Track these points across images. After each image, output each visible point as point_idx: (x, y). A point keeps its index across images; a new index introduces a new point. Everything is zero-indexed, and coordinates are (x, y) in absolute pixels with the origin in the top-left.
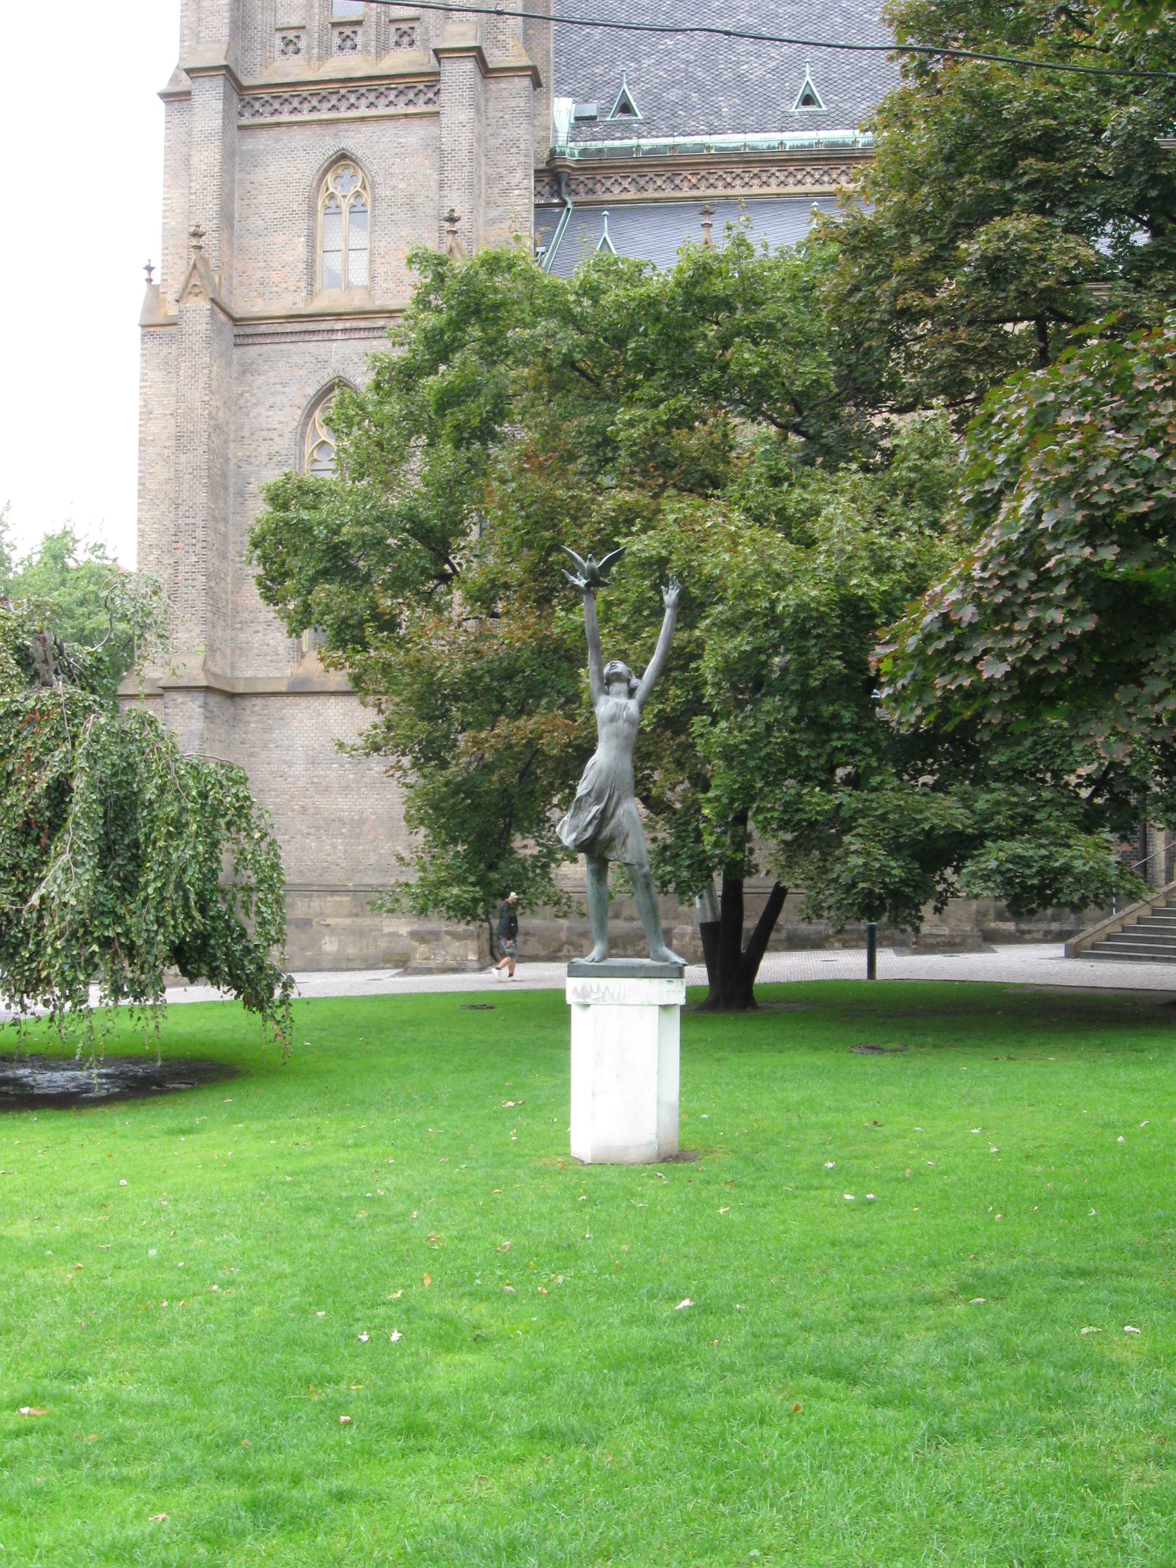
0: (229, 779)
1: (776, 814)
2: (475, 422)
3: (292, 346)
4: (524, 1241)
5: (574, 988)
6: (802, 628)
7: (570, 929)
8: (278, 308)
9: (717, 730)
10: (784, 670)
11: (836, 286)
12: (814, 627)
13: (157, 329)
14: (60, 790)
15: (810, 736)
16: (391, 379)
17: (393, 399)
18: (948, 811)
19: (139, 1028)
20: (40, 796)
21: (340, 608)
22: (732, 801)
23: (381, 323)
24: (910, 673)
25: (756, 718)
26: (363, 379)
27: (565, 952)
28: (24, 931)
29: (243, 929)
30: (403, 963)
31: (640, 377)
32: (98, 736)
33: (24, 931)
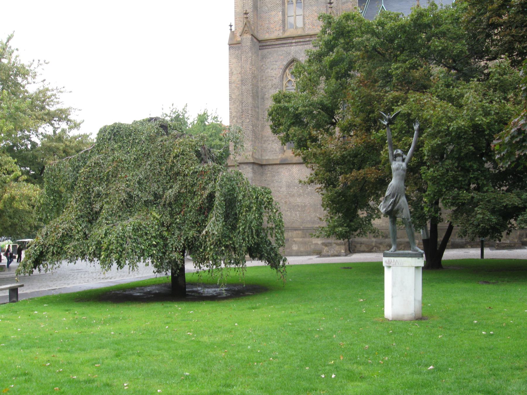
0: (265, 192)
1: (450, 201)
2: (343, 71)
3: (278, 49)
4: (373, 346)
5: (385, 260)
6: (459, 135)
7: (376, 242)
8: (273, 36)
9: (430, 171)
10: (452, 151)
11: (467, 17)
12: (463, 135)
13: (234, 46)
14: (211, 197)
15: (462, 173)
16: (314, 58)
17: (314, 64)
18: (513, 199)
19: (237, 275)
20: (204, 199)
21: (299, 135)
22: (434, 196)
23: (308, 39)
24: (506, 150)
25: (443, 167)
26: (303, 58)
27: (374, 249)
28: (200, 243)
29: (270, 242)
30: (319, 254)
31: (399, 53)
32: (223, 179)
33: (200, 243)
